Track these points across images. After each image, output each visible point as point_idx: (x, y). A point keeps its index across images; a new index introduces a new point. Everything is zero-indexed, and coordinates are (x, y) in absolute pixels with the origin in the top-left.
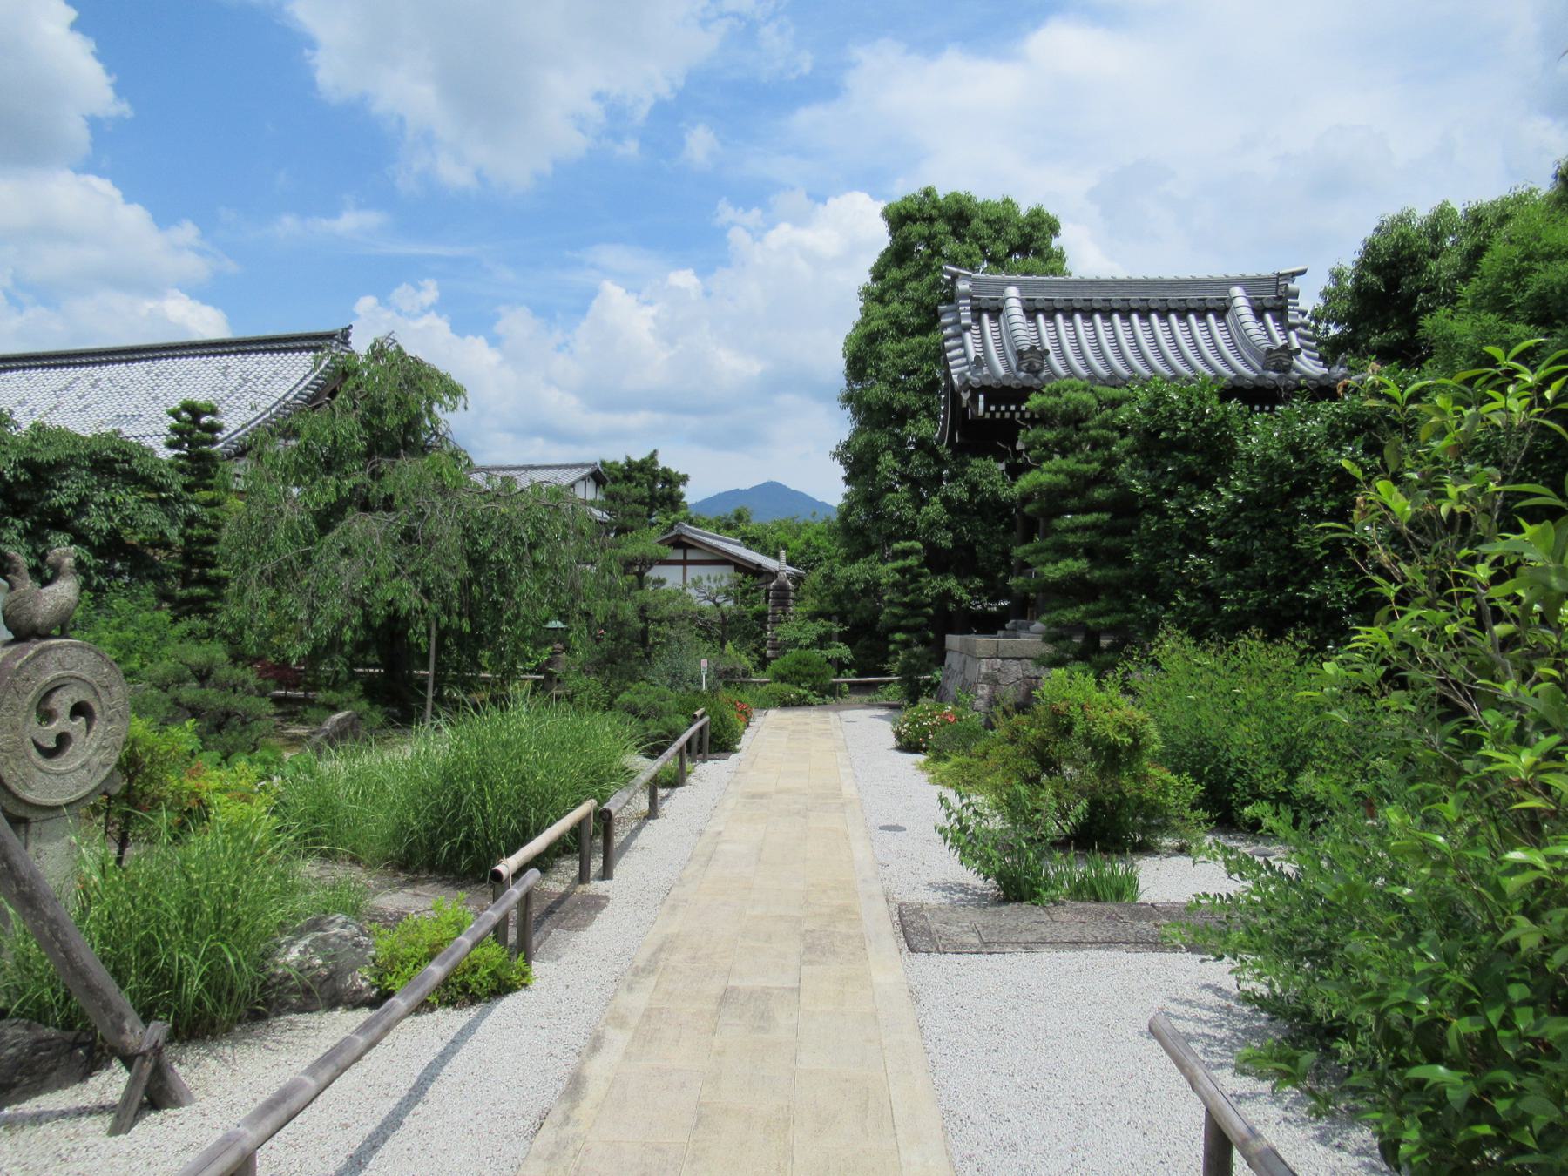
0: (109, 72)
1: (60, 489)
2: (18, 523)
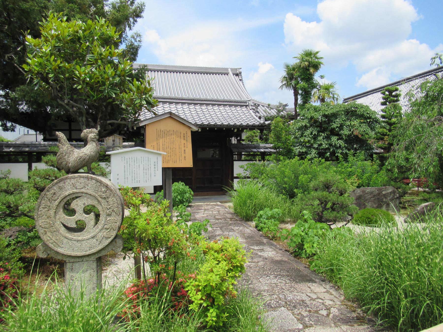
0: (415, 8)
1: (335, 122)
2: (323, 134)
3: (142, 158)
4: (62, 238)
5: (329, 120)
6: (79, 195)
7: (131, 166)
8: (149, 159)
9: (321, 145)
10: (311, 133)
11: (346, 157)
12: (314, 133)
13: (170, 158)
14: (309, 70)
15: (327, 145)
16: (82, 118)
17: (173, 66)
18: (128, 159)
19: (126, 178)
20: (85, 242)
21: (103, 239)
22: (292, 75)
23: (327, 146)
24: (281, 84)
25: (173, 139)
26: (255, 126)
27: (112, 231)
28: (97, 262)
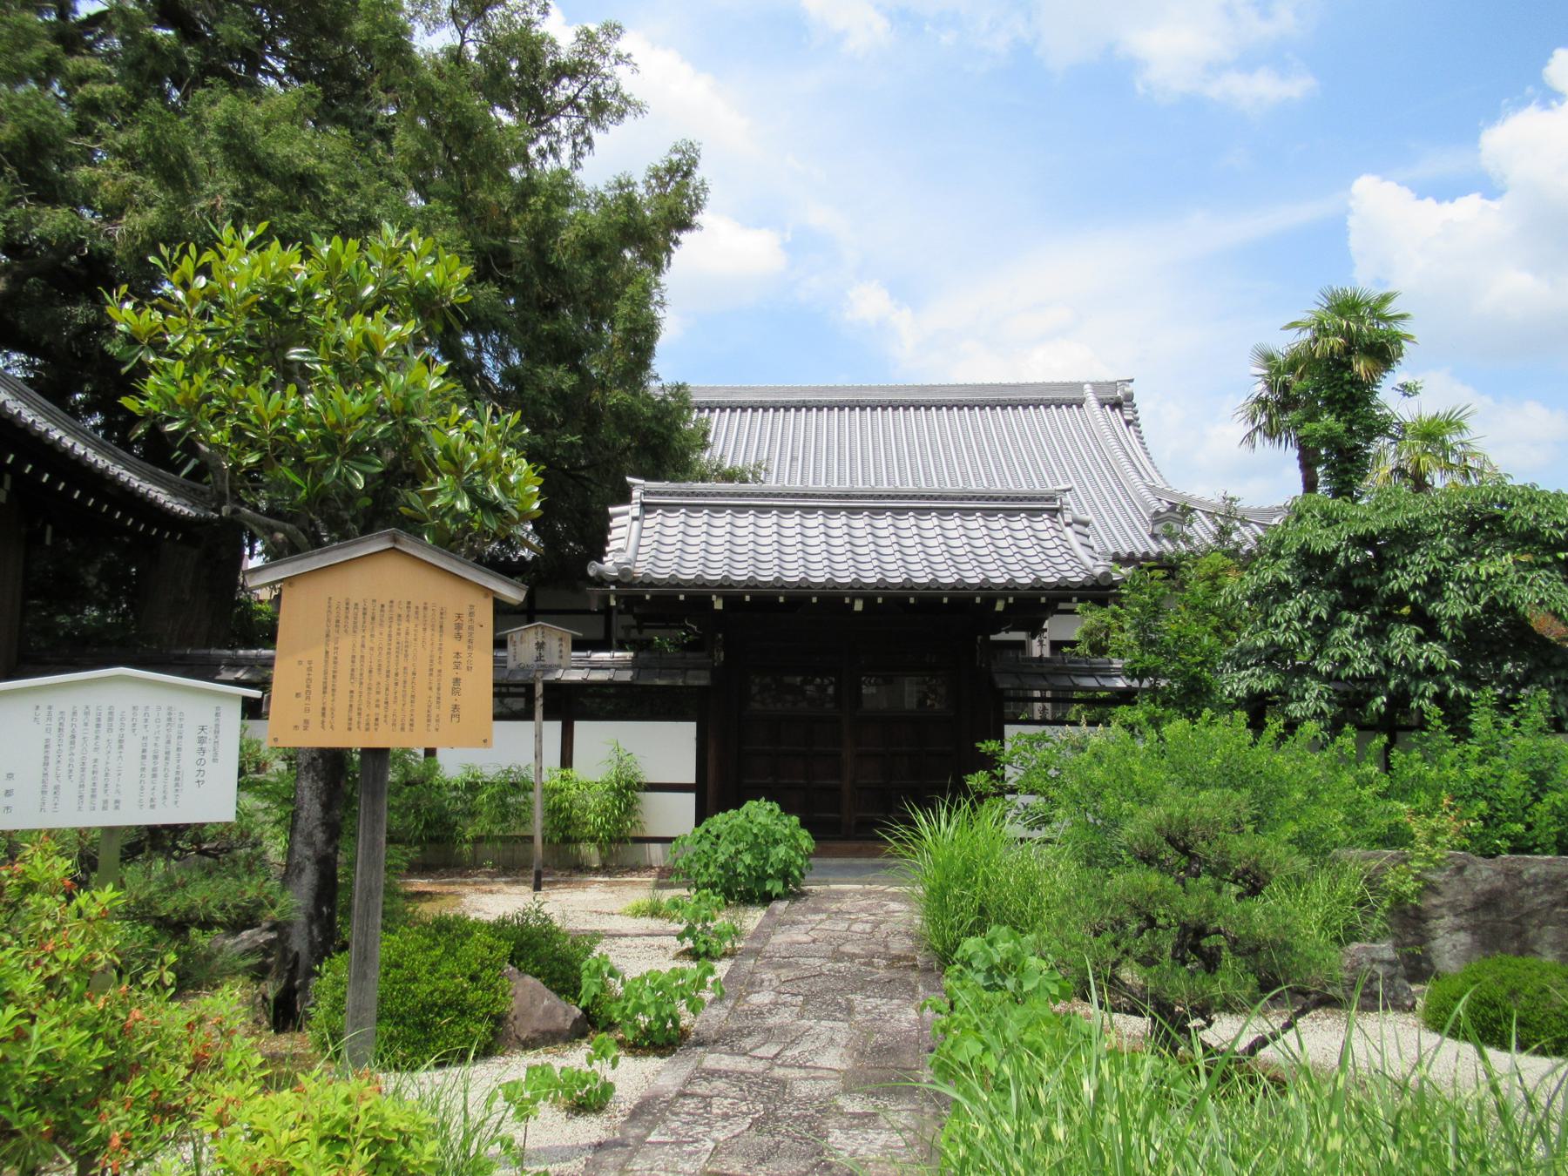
1: (1404, 567)
2: (1355, 618)
3: (140, 712)
5: (1379, 556)
7: (79, 740)
8: (176, 716)
9: (1346, 661)
10: (1303, 617)
11: (1457, 716)
12: (1312, 615)
13: (381, 711)
14: (1349, 367)
15: (1372, 660)
17: (908, 389)
22: (1285, 388)
23: (1373, 668)
24: (1250, 428)
26: (1067, 588)
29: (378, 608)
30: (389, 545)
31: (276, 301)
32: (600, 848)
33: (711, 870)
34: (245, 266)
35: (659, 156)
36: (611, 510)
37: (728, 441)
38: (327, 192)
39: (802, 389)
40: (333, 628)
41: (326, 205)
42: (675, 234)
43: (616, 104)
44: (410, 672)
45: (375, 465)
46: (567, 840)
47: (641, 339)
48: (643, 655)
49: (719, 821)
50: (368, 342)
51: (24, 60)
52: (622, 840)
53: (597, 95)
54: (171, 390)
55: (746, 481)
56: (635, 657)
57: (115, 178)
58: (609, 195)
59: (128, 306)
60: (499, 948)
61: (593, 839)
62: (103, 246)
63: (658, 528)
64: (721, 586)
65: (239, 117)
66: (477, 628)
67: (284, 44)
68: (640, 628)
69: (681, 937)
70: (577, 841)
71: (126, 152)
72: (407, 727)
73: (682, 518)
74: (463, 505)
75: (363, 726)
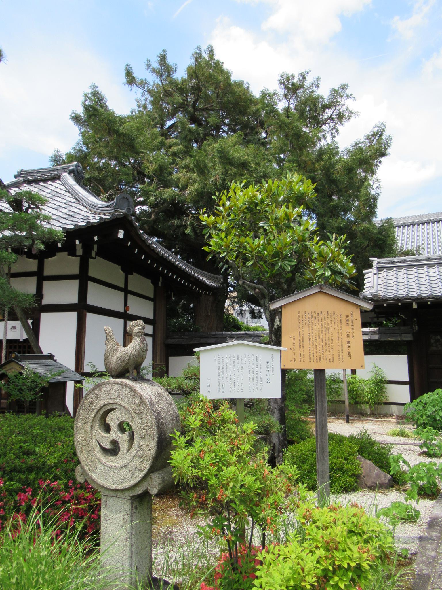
4: (97, 461)
6: (114, 407)
7: (228, 367)
13: (321, 355)
16: (265, 301)
18: (225, 358)
19: (221, 385)
20: (117, 470)
21: (135, 470)
25: (326, 326)
27: (145, 461)
28: (132, 503)
29: (317, 314)
30: (319, 290)
31: (251, 206)
32: (370, 407)
33: (424, 417)
34: (241, 194)
35: (369, 131)
36: (364, 271)
37: (403, 239)
38: (251, 167)
39: (429, 215)
40: (301, 323)
41: (251, 172)
42: (380, 159)
43: (347, 114)
44: (330, 339)
45: (293, 262)
46: (357, 403)
47: (371, 204)
48: (381, 329)
49: (426, 397)
50: (287, 216)
51: (155, 143)
52: (379, 403)
53: (340, 113)
54: (220, 242)
55: (413, 255)
56: (379, 329)
57: (184, 175)
58: (351, 149)
59: (206, 215)
60: (354, 447)
61: (367, 403)
62: (182, 198)
63: (385, 277)
64: (417, 298)
65: (223, 146)
66: (355, 321)
67: (227, 121)
68: (378, 318)
69: (421, 446)
70: (361, 403)
71: (186, 167)
72: (331, 361)
73: (395, 272)
74: (328, 273)
75: (315, 361)
